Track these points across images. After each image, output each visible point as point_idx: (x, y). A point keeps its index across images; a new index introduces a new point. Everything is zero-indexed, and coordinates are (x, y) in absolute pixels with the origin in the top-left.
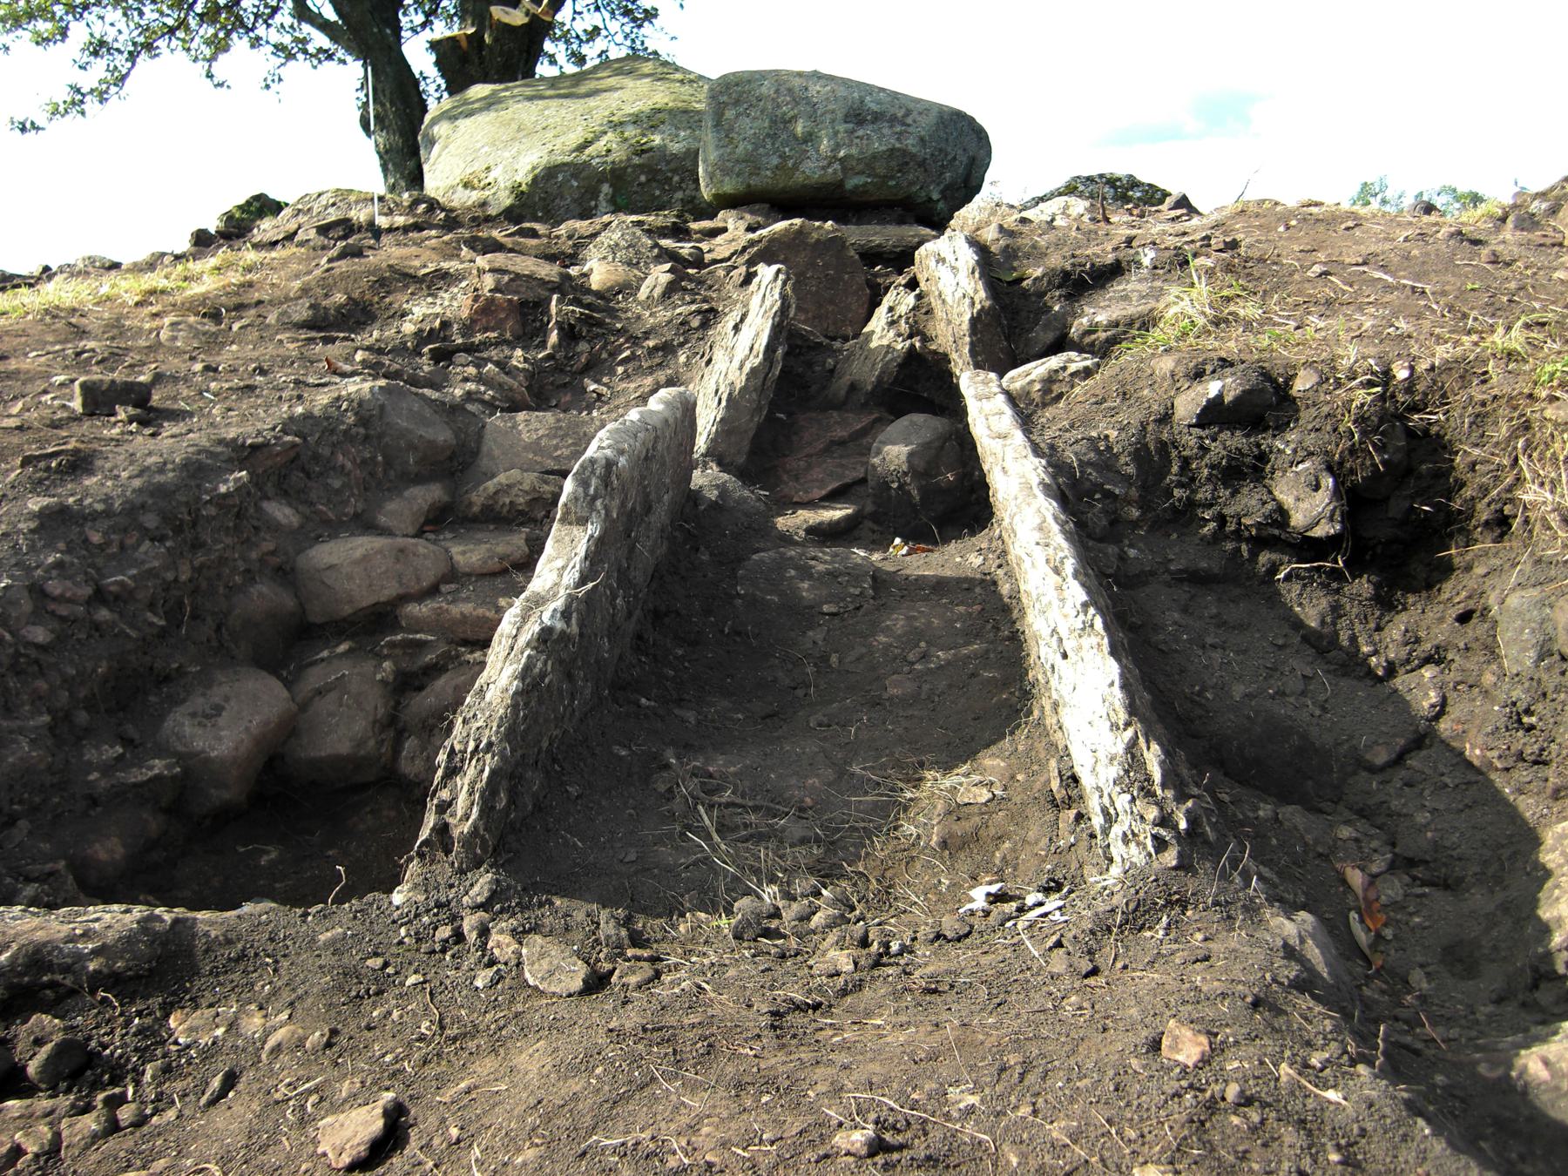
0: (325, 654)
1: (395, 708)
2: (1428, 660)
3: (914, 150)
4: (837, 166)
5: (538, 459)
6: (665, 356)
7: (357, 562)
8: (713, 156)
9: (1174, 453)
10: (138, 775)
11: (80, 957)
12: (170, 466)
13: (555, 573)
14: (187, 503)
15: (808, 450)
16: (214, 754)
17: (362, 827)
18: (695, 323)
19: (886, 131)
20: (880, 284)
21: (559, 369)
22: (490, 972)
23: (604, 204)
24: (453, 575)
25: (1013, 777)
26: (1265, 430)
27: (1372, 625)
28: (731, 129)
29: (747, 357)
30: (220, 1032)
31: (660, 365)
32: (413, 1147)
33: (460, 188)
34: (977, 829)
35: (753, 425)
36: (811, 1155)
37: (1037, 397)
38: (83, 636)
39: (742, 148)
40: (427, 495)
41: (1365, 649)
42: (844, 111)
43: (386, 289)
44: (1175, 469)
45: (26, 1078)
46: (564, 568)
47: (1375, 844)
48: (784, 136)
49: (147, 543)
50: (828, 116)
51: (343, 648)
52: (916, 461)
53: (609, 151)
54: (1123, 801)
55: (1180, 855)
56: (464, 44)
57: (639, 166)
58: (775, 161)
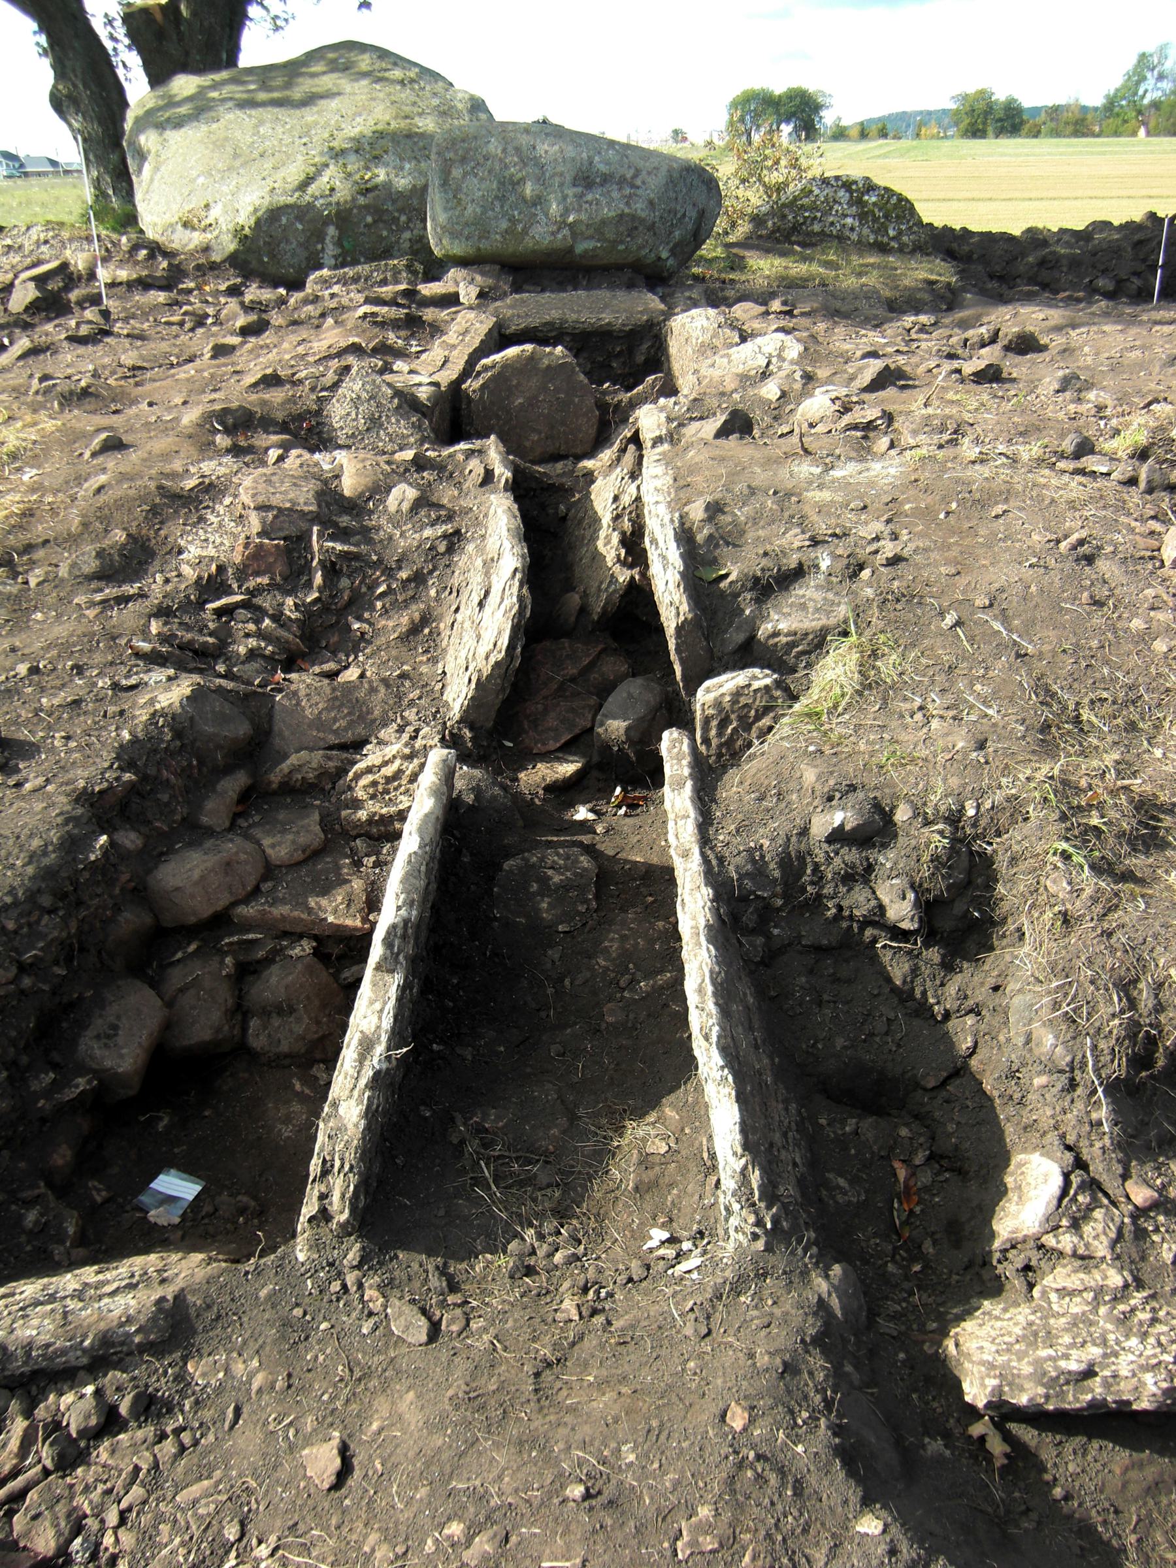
0: (179, 955)
1: (240, 997)
2: (971, 1011)
3: (643, 215)
4: (566, 231)
5: (321, 735)
6: (417, 587)
7: (196, 883)
8: (442, 218)
9: (809, 860)
10: (71, 1094)
11: (128, 1335)
12: (50, 848)
13: (376, 1016)
14: (69, 878)
15: (545, 692)
16: (121, 1070)
17: (225, 1088)
18: (442, 548)
19: (615, 194)
20: (609, 405)
21: (326, 609)
22: (372, 1321)
23: (331, 247)
24: (270, 871)
25: (683, 1130)
26: (874, 846)
27: (938, 982)
28: (458, 189)
29: (492, 651)
30: (221, 1375)
31: (413, 597)
32: (357, 1474)
33: (179, 227)
34: (658, 1177)
35: (498, 702)
36: (556, 1501)
37: (727, 706)
38: (14, 1003)
39: (471, 210)
40: (233, 784)
41: (932, 1001)
42: (573, 174)
43: (159, 518)
44: (809, 871)
45: (119, 1415)
46: (381, 1011)
47: (922, 1140)
48: (513, 198)
49: (46, 917)
50: (557, 179)
51: (192, 948)
52: (632, 734)
53: (332, 190)
54: (736, 1207)
55: (767, 1243)
56: (159, 17)
57: (366, 207)
58: (504, 225)
